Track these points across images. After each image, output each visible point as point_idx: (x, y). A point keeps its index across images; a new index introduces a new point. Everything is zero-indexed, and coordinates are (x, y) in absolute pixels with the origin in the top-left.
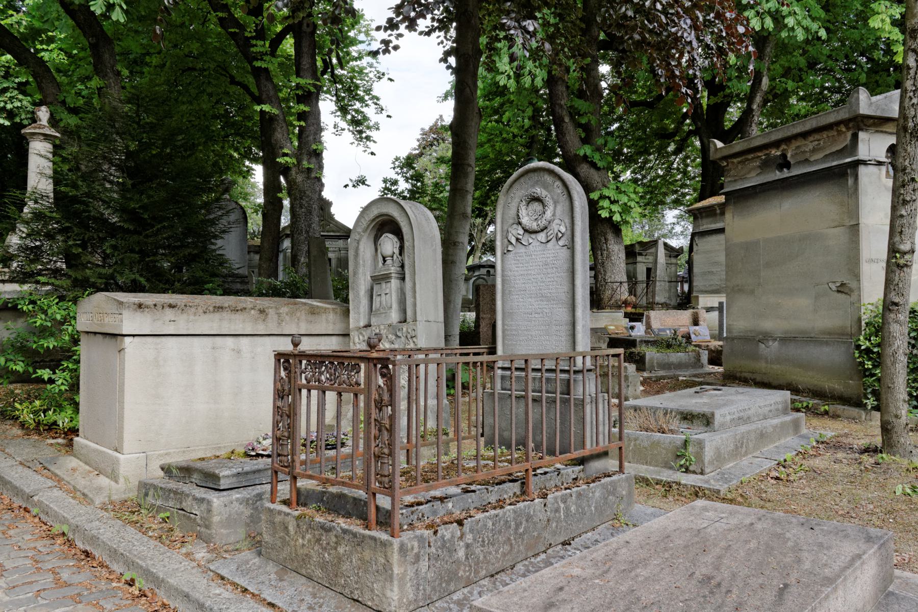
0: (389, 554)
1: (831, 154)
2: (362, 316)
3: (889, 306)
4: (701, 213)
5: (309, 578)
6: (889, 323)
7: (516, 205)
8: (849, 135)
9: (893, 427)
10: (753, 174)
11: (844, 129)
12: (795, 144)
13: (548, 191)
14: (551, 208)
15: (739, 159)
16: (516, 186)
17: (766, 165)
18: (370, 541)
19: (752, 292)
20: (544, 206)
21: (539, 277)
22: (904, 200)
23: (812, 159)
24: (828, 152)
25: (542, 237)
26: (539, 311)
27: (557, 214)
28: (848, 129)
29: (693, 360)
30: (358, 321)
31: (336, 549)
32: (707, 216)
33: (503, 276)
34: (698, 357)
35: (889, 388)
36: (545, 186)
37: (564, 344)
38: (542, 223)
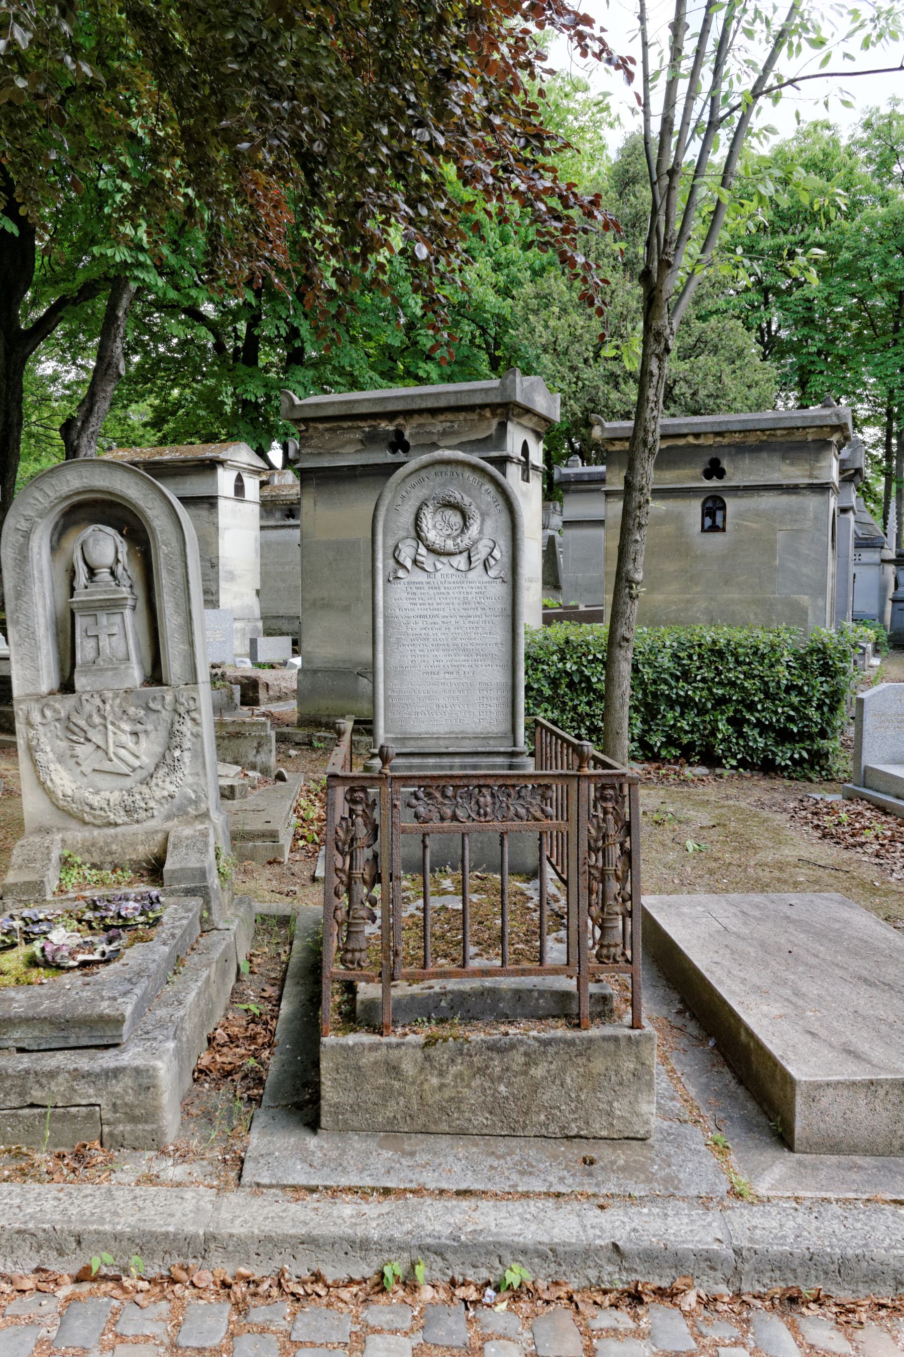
0: (645, 1055)
1: (470, 442)
2: (44, 673)
3: (614, 641)
5: (462, 1133)
7: (414, 510)
8: (495, 423)
10: (350, 449)
11: (488, 415)
12: (417, 420)
13: (470, 496)
15: (328, 425)
16: (413, 480)
17: (371, 440)
18: (605, 1045)
19: (347, 609)
23: (441, 444)
24: (465, 439)
25: (460, 561)
26: (450, 669)
28: (494, 415)
30: (35, 681)
31: (525, 1073)
34: (231, 697)
37: (494, 716)
38: (464, 542)
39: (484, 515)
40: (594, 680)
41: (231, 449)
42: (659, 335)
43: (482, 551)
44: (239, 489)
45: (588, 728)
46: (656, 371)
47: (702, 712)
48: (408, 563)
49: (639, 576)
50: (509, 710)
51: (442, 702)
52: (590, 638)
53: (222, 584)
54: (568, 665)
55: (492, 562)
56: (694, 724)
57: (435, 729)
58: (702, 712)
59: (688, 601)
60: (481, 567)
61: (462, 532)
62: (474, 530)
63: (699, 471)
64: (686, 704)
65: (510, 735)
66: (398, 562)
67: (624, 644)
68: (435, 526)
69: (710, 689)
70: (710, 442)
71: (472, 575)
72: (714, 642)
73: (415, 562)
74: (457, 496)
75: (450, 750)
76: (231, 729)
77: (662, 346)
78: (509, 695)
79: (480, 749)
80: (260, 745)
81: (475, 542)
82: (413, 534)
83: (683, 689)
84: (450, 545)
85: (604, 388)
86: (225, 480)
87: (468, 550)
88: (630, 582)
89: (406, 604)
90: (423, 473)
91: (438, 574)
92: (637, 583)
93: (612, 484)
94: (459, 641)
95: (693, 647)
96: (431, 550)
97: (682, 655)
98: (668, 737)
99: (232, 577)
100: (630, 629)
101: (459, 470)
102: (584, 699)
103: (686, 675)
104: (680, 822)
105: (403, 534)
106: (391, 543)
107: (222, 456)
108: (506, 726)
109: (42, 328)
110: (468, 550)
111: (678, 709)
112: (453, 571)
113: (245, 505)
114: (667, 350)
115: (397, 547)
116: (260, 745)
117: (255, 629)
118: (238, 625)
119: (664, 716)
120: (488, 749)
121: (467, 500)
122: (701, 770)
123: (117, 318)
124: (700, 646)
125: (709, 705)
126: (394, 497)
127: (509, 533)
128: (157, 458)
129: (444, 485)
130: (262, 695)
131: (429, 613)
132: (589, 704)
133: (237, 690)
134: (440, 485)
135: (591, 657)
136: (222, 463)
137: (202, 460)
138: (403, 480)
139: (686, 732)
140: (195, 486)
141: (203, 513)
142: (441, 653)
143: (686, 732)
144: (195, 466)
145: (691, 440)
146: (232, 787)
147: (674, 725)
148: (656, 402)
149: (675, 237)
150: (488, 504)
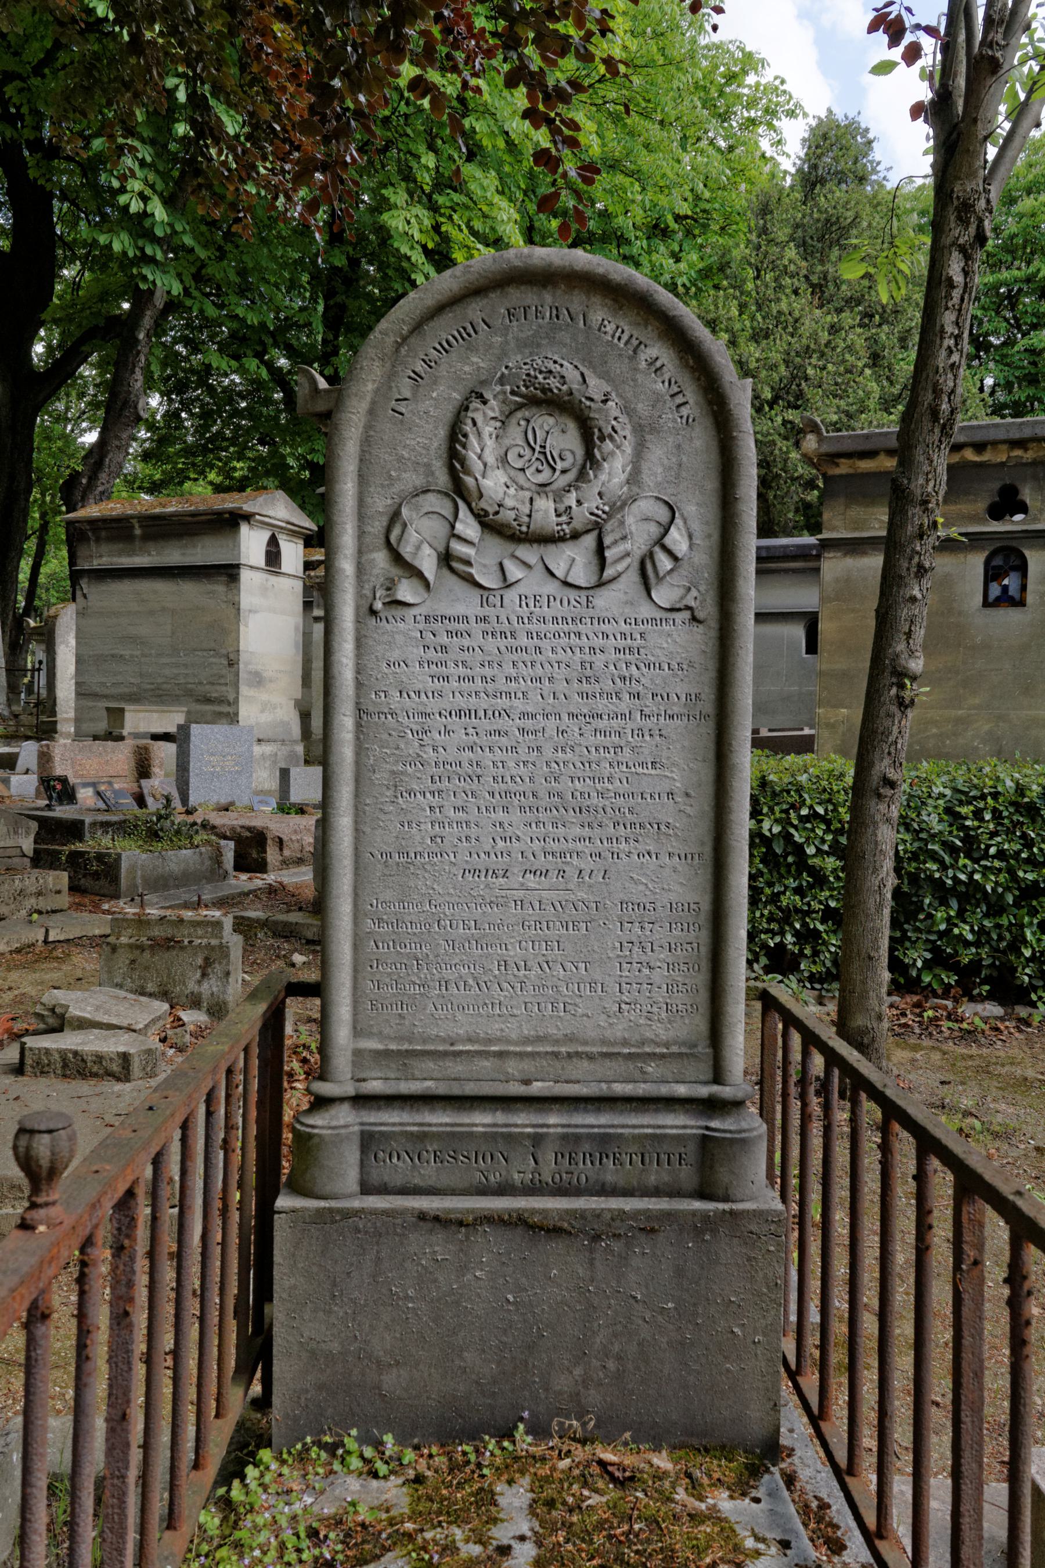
3: (865, 788)
4: (94, 530)
6: (875, 824)
7: (447, 413)
9: (873, 1040)
13: (605, 376)
14: (628, 448)
16: (444, 328)
20: (590, 436)
21: (551, 724)
22: (920, 566)
25: (574, 561)
26: (541, 862)
27: (646, 478)
29: (208, 863)
32: (111, 539)
33: (360, 711)
34: (217, 858)
35: (870, 958)
36: (591, 358)
38: (587, 504)
39: (642, 432)
40: (811, 850)
41: (261, 499)
42: (966, 208)
43: (636, 532)
44: (273, 557)
45: (796, 934)
46: (958, 279)
47: (996, 909)
48: (428, 563)
49: (916, 665)
50: (701, 979)
51: (515, 953)
52: (803, 778)
53: (244, 690)
54: (766, 825)
55: (665, 563)
56: (982, 931)
57: (495, 1028)
58: (996, 909)
59: (958, 721)
60: (632, 577)
61: (582, 476)
62: (614, 472)
63: (981, 506)
64: (969, 895)
65: (704, 1049)
66: (397, 558)
67: (887, 791)
68: (504, 460)
69: (1011, 872)
70: (1003, 458)
71: (606, 600)
72: (1020, 790)
73: (446, 559)
74: (570, 374)
75: (537, 1088)
76: (157, 932)
77: (972, 230)
78: (704, 936)
79: (621, 1089)
80: (208, 962)
81: (618, 507)
82: (442, 479)
83: (964, 870)
84: (546, 513)
85: (782, 444)
86: (252, 544)
87: (597, 527)
88: (901, 675)
89: (420, 678)
90: (475, 310)
91: (511, 595)
92: (914, 678)
93: (833, 529)
94: (565, 785)
95: (983, 797)
96: (490, 525)
97: (964, 810)
98: (935, 950)
99: (258, 680)
100: (896, 764)
101: (577, 301)
102: (792, 883)
103: (971, 846)
104: (996, 1135)
105: (413, 479)
106: (381, 504)
107: (247, 508)
108: (699, 1024)
109: (62, 370)
110: (597, 527)
111: (954, 904)
112: (552, 588)
113: (281, 580)
114: (981, 239)
115: (395, 516)
116: (208, 962)
117: (292, 756)
118: (268, 749)
119: (930, 916)
120: (641, 1089)
121: (596, 386)
122: (993, 1009)
123: (137, 341)
124: (995, 795)
125: (1010, 899)
126: (391, 376)
127: (712, 485)
128: (157, 510)
129: (531, 345)
130: (272, 855)
131: (484, 703)
132: (799, 891)
133: (229, 849)
134: (523, 345)
135: (804, 812)
136: (248, 517)
137: (219, 514)
138: (417, 328)
139: (967, 944)
140: (205, 552)
141: (220, 588)
142: (516, 816)
143: (967, 944)
144: (209, 522)
145: (970, 455)
146: (125, 1057)
147: (948, 932)
148: (958, 338)
149: (1007, 18)
150: (657, 400)
